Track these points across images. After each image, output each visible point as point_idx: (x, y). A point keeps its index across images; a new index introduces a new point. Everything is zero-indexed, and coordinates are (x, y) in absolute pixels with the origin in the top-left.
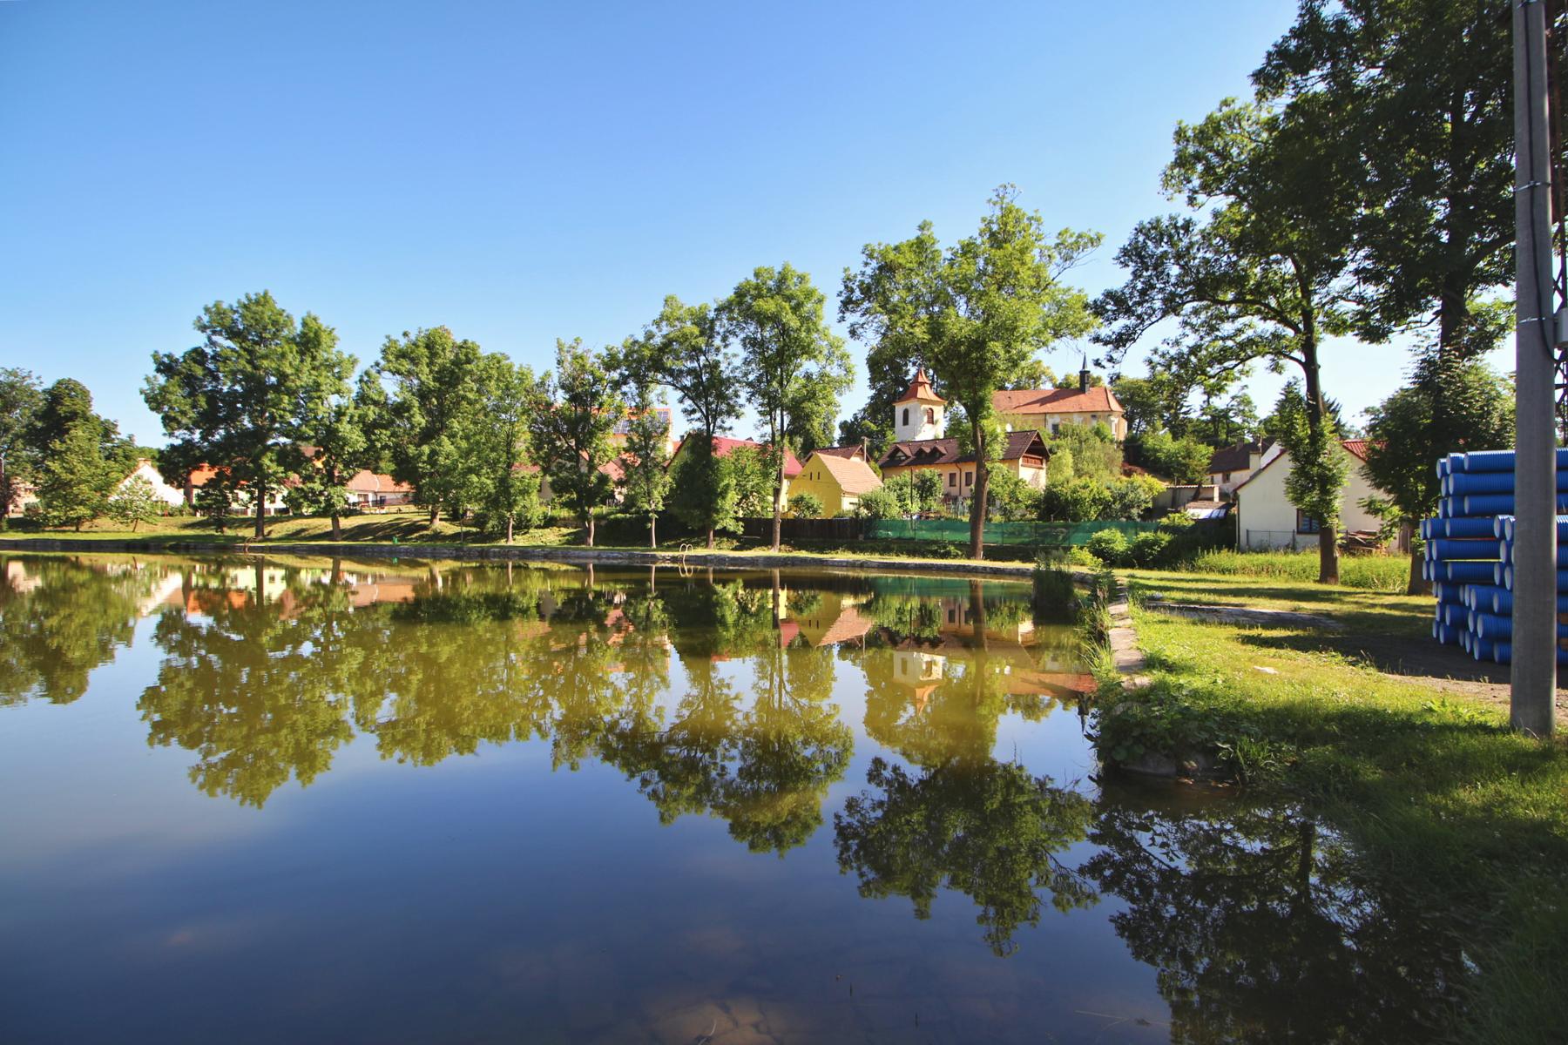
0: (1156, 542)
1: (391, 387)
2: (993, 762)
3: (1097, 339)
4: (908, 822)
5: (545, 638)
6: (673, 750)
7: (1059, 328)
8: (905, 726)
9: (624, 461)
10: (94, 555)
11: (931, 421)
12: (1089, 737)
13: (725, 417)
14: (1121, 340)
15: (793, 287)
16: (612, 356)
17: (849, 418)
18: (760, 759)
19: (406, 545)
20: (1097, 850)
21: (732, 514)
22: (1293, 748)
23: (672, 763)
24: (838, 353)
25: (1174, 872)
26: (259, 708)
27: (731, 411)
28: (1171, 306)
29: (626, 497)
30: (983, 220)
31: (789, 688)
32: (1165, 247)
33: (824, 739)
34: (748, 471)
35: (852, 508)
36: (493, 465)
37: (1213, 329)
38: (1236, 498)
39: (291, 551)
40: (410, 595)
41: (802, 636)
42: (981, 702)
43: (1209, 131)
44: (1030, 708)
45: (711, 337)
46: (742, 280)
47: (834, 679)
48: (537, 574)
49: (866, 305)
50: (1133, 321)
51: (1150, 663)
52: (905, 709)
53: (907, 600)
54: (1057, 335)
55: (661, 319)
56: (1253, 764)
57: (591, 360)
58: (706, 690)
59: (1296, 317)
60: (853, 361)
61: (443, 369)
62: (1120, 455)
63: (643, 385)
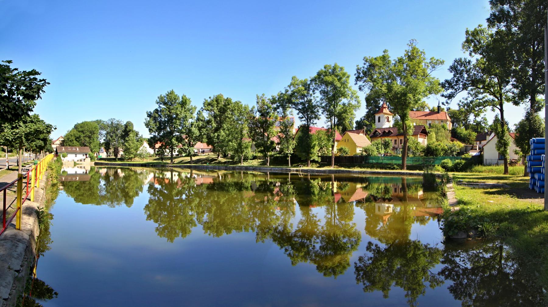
0: (461, 163)
1: (206, 115)
2: (410, 240)
3: (443, 96)
4: (381, 264)
5: (253, 197)
6: (296, 239)
7: (431, 91)
8: (380, 230)
9: (279, 136)
10: (135, 168)
11: (388, 121)
12: (441, 229)
13: (314, 120)
14: (450, 97)
15: (338, 72)
16: (274, 99)
17: (359, 120)
18: (327, 243)
19: (211, 165)
20: (443, 266)
21: (317, 154)
22: (498, 224)
23: (296, 244)
24: (355, 96)
25: (466, 268)
26: (172, 214)
27: (316, 117)
28: (465, 87)
29: (280, 149)
30: (406, 51)
31: (338, 217)
32: (463, 68)
33: (351, 235)
34: (322, 139)
35: (360, 152)
36: (236, 139)
37: (476, 96)
38: (483, 149)
39: (180, 167)
40: (212, 181)
41: (342, 198)
42: (406, 220)
43: (475, 33)
44: (422, 220)
45: (309, 90)
46: (320, 70)
47: (354, 214)
48: (250, 175)
49: (365, 79)
50: (453, 91)
51: (459, 202)
52: (379, 224)
53: (380, 185)
54: (430, 93)
55: (291, 85)
56: (488, 231)
57: (267, 101)
58: (308, 218)
59: (498, 96)
60: (360, 99)
61: (221, 108)
62: (450, 135)
63: (284, 109)
